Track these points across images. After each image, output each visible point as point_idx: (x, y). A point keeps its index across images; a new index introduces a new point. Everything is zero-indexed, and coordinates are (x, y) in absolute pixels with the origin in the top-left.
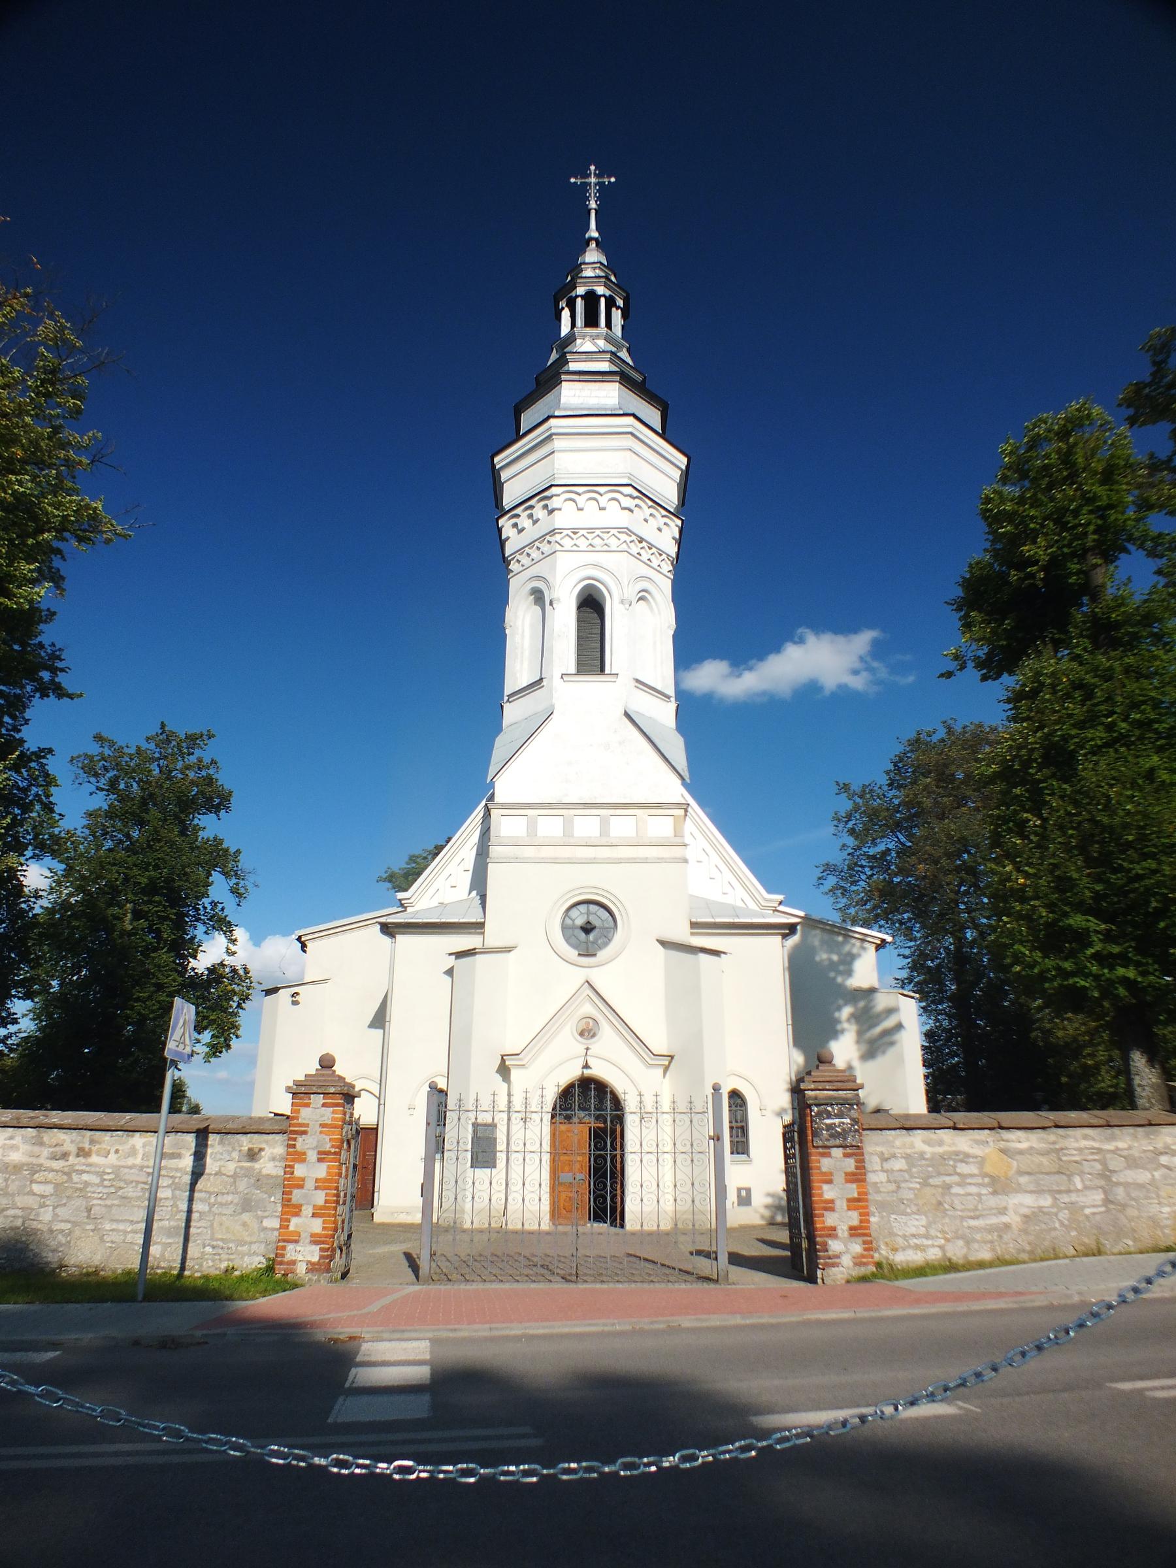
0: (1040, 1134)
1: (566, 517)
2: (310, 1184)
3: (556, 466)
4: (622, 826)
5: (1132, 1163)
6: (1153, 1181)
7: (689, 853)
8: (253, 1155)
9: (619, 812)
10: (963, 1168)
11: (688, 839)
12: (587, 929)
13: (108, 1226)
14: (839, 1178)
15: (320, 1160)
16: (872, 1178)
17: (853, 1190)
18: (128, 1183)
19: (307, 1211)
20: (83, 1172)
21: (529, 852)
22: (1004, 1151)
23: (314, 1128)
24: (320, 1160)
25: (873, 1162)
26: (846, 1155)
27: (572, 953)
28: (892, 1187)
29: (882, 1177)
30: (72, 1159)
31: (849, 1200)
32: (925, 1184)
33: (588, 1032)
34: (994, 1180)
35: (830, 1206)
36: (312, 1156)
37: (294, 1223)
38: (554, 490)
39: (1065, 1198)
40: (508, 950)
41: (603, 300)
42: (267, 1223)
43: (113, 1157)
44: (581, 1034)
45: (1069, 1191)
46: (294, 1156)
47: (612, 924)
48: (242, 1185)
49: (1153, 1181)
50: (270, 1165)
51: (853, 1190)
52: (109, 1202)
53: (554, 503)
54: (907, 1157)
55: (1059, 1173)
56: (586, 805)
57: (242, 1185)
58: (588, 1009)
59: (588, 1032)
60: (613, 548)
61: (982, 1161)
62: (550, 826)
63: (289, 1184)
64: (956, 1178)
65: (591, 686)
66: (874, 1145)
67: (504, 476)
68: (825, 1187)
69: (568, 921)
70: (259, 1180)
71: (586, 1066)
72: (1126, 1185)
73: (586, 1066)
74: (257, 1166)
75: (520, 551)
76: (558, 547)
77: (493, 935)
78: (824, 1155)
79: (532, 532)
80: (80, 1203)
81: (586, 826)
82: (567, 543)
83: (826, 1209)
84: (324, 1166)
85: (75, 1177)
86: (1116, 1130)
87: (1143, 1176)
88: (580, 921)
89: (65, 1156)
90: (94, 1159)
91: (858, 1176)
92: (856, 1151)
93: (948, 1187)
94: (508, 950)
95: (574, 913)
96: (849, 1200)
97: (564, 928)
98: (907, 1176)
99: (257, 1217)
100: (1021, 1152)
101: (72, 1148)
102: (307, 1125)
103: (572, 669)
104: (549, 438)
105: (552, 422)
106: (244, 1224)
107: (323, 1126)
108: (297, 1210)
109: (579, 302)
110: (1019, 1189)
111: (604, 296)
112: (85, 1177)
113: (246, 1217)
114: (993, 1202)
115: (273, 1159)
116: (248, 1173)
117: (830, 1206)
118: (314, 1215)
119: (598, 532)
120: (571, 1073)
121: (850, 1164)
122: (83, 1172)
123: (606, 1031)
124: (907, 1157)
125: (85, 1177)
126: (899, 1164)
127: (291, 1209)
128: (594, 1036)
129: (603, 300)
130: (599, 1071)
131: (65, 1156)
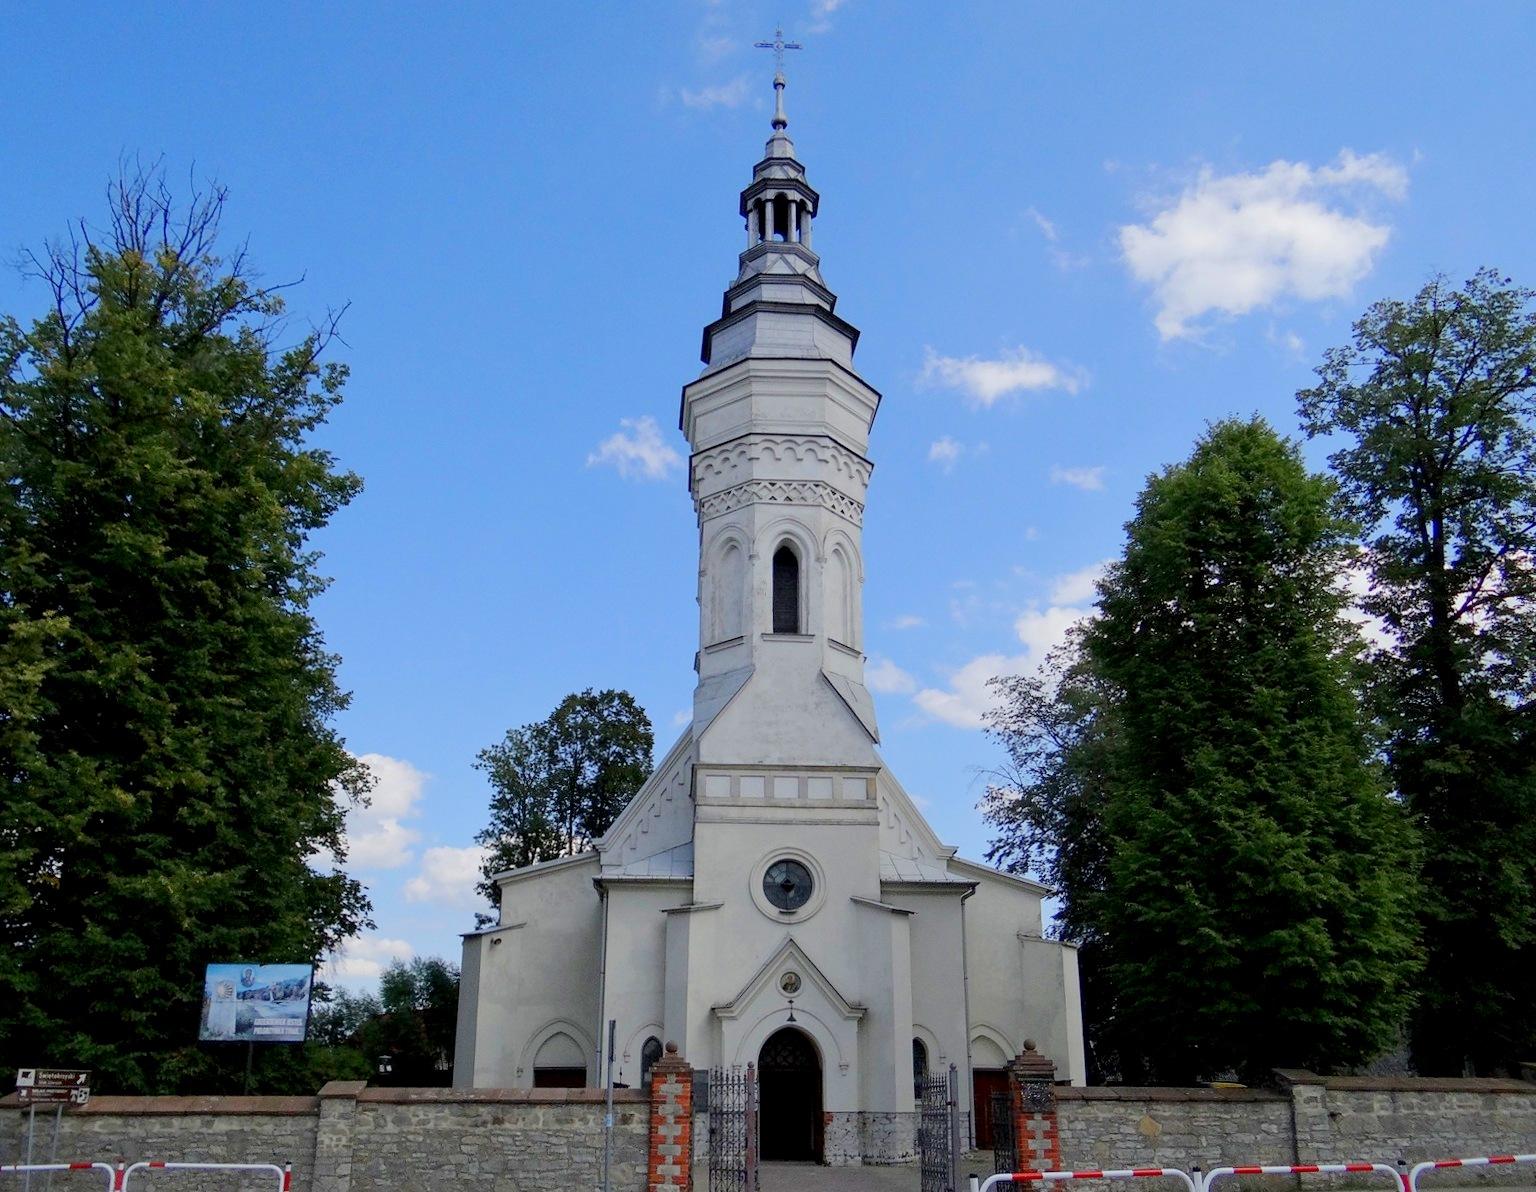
0: (1179, 1107)
1: (764, 468)
2: (671, 1140)
3: (754, 411)
4: (819, 789)
5: (1242, 1129)
6: (1256, 1142)
7: (881, 818)
8: (626, 1120)
9: (816, 774)
10: (1125, 1129)
11: (879, 803)
12: (786, 887)
13: (521, 1175)
14: (1039, 1134)
15: (676, 1123)
16: (1062, 1135)
17: (1048, 1144)
18: (535, 1143)
19: (670, 1159)
20: (498, 1135)
21: (734, 813)
22: (1153, 1117)
23: (671, 1098)
24: (676, 1123)
25: (1063, 1124)
26: (1044, 1119)
27: (773, 911)
28: (1075, 1141)
29: (1069, 1134)
30: (489, 1126)
31: (1045, 1151)
32: (1098, 1139)
33: (791, 985)
34: (1146, 1138)
35: (1033, 1155)
36: (671, 1119)
37: (660, 1169)
38: (752, 439)
39: (1195, 1153)
40: (717, 907)
41: (794, 208)
42: (638, 1170)
43: (520, 1124)
44: (785, 988)
45: (1196, 1148)
46: (653, 1121)
47: (800, 872)
48: (620, 1142)
49: (1256, 1142)
50: (637, 1127)
51: (1048, 1144)
52: (521, 1157)
53: (754, 452)
54: (1086, 1120)
55: (1190, 1134)
56: (786, 768)
57: (620, 1142)
58: (791, 965)
59: (791, 985)
60: (810, 502)
61: (1137, 1125)
62: (752, 787)
63: (651, 1140)
64: (1120, 1137)
65: (786, 646)
66: (1064, 1112)
67: (697, 409)
68: (1030, 1141)
69: (769, 880)
70: (631, 1136)
71: (791, 1019)
72: (1238, 1144)
73: (791, 1019)
74: (628, 1127)
75: (716, 495)
76: (756, 500)
77: (702, 892)
78: (1028, 1118)
79: (729, 478)
80: (500, 1158)
81: (786, 788)
82: (764, 493)
83: (1030, 1157)
84: (680, 1127)
85: (494, 1139)
86: (1233, 1106)
87: (1248, 1138)
88: (780, 879)
89: (484, 1123)
90: (507, 1125)
91: (1051, 1134)
92: (1050, 1115)
93: (1113, 1142)
94: (717, 907)
95: (774, 873)
96: (1045, 1151)
97: (767, 887)
98: (1085, 1133)
99: (632, 1165)
100: (1166, 1118)
101: (489, 1118)
102: (665, 1097)
103: (770, 630)
104: (747, 380)
105: (752, 364)
106: (623, 1171)
107: (676, 1096)
108: (662, 1160)
109: (769, 209)
110: (1164, 1145)
111: (794, 201)
112: (501, 1139)
113: (623, 1165)
114: (1145, 1153)
115: (641, 1122)
116: (623, 1133)
117: (1033, 1155)
118: (674, 1163)
119: (794, 484)
120: (779, 1022)
121: (1047, 1125)
122: (498, 1135)
123: (806, 985)
124: (1086, 1120)
125: (501, 1139)
126: (1080, 1125)
127: (654, 1159)
128: (796, 989)
129: (794, 208)
130: (803, 1022)
131: (484, 1123)
